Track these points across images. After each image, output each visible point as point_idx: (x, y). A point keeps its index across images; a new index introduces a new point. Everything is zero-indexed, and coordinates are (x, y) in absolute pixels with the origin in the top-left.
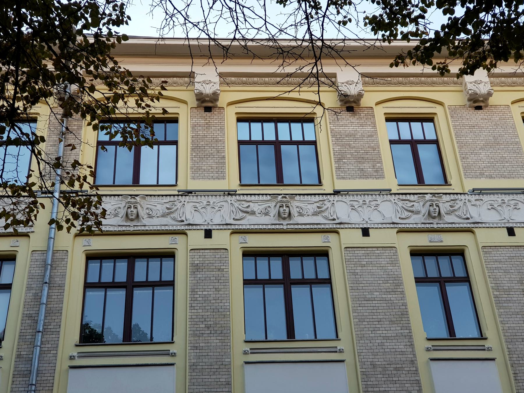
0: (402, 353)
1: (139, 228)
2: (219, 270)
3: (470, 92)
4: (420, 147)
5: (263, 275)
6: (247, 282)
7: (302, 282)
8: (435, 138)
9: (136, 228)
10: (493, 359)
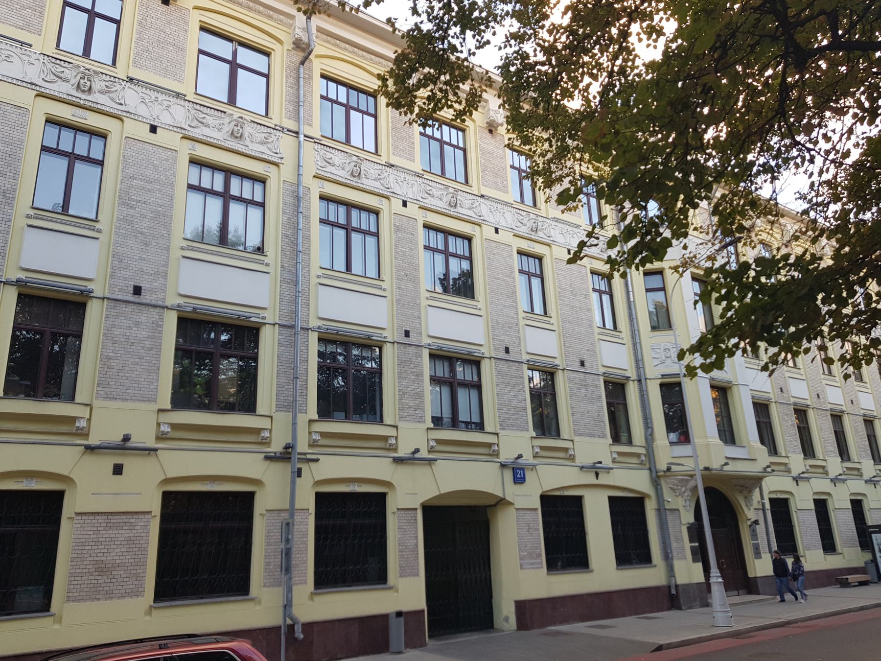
0: (512, 318)
1: (360, 185)
2: (412, 234)
3: (297, 36)
4: (352, 112)
5: (206, 184)
6: (44, 149)
7: (240, 199)
9: (357, 184)
10: (385, 297)
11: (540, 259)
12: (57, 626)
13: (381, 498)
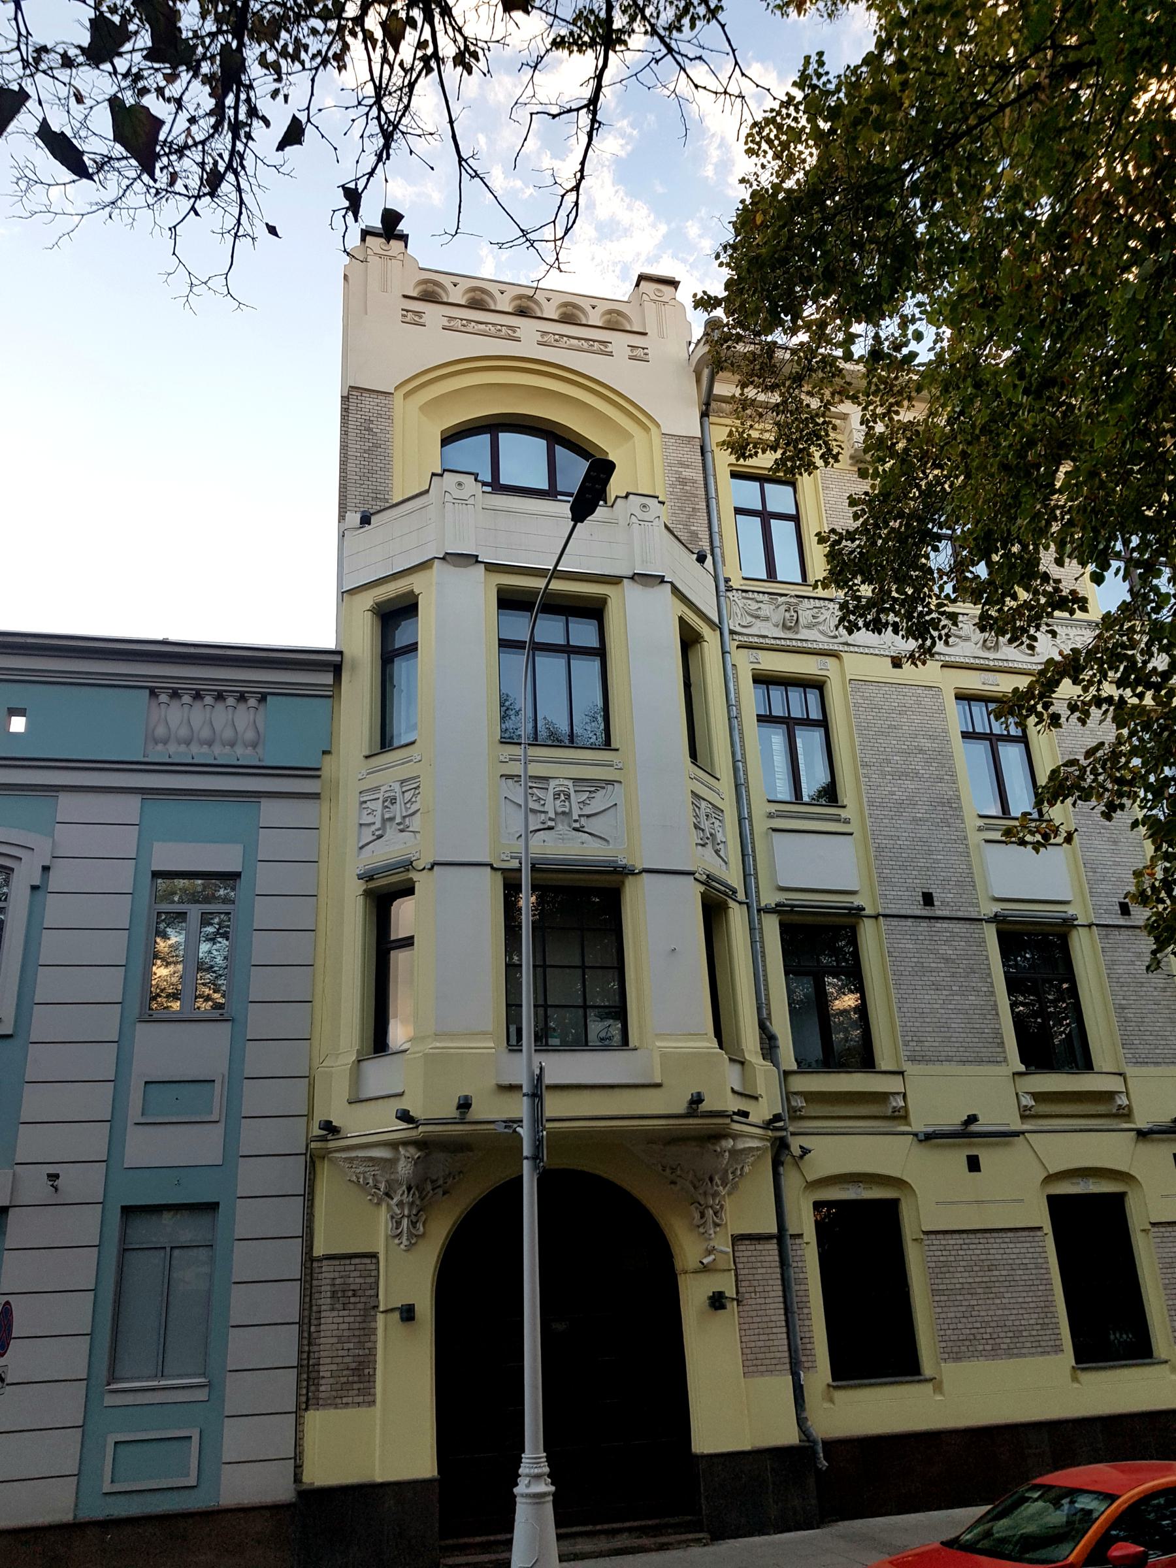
8: (794, 512)
10: (851, 834)
11: (818, 685)
12: (939, 1398)
13: (890, 1209)
